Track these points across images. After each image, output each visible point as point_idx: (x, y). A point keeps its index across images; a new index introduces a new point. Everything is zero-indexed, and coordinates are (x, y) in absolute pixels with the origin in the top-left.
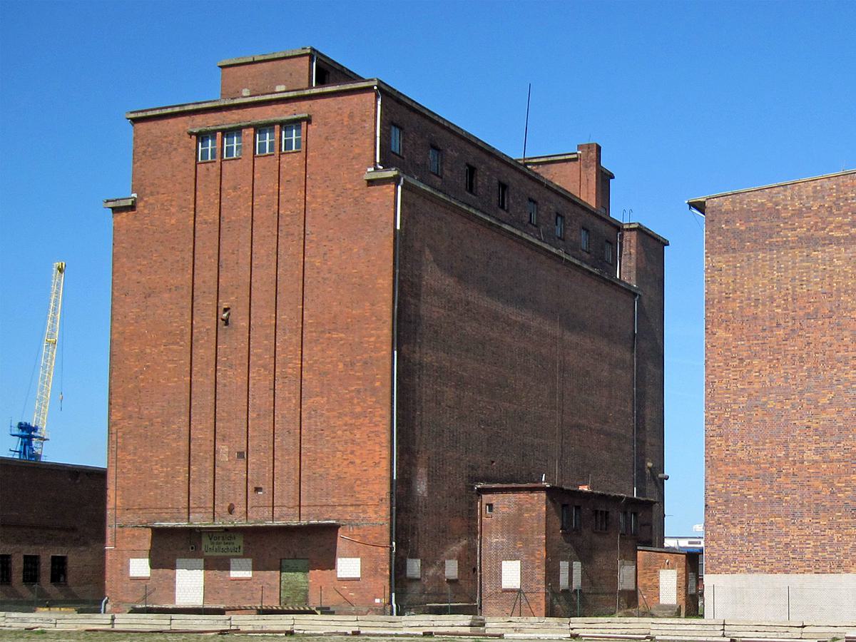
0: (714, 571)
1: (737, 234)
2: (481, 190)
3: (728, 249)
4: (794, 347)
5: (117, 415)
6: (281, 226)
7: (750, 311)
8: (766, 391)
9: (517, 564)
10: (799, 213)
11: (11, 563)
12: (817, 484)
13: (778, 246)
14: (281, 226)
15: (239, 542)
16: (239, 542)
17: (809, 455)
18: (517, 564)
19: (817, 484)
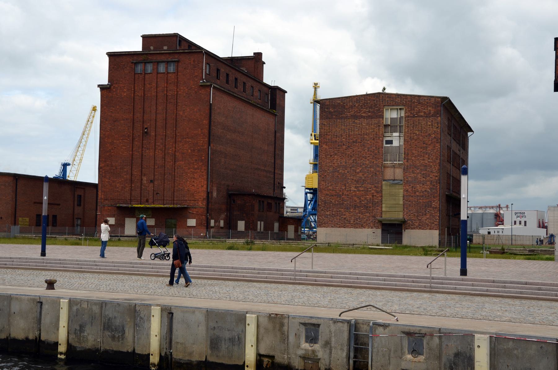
1: (330, 112)
5: (102, 165)
9: (243, 222)
10: (352, 107)
12: (355, 198)
13: (347, 118)
17: (353, 189)
18: (243, 222)
19: (355, 198)
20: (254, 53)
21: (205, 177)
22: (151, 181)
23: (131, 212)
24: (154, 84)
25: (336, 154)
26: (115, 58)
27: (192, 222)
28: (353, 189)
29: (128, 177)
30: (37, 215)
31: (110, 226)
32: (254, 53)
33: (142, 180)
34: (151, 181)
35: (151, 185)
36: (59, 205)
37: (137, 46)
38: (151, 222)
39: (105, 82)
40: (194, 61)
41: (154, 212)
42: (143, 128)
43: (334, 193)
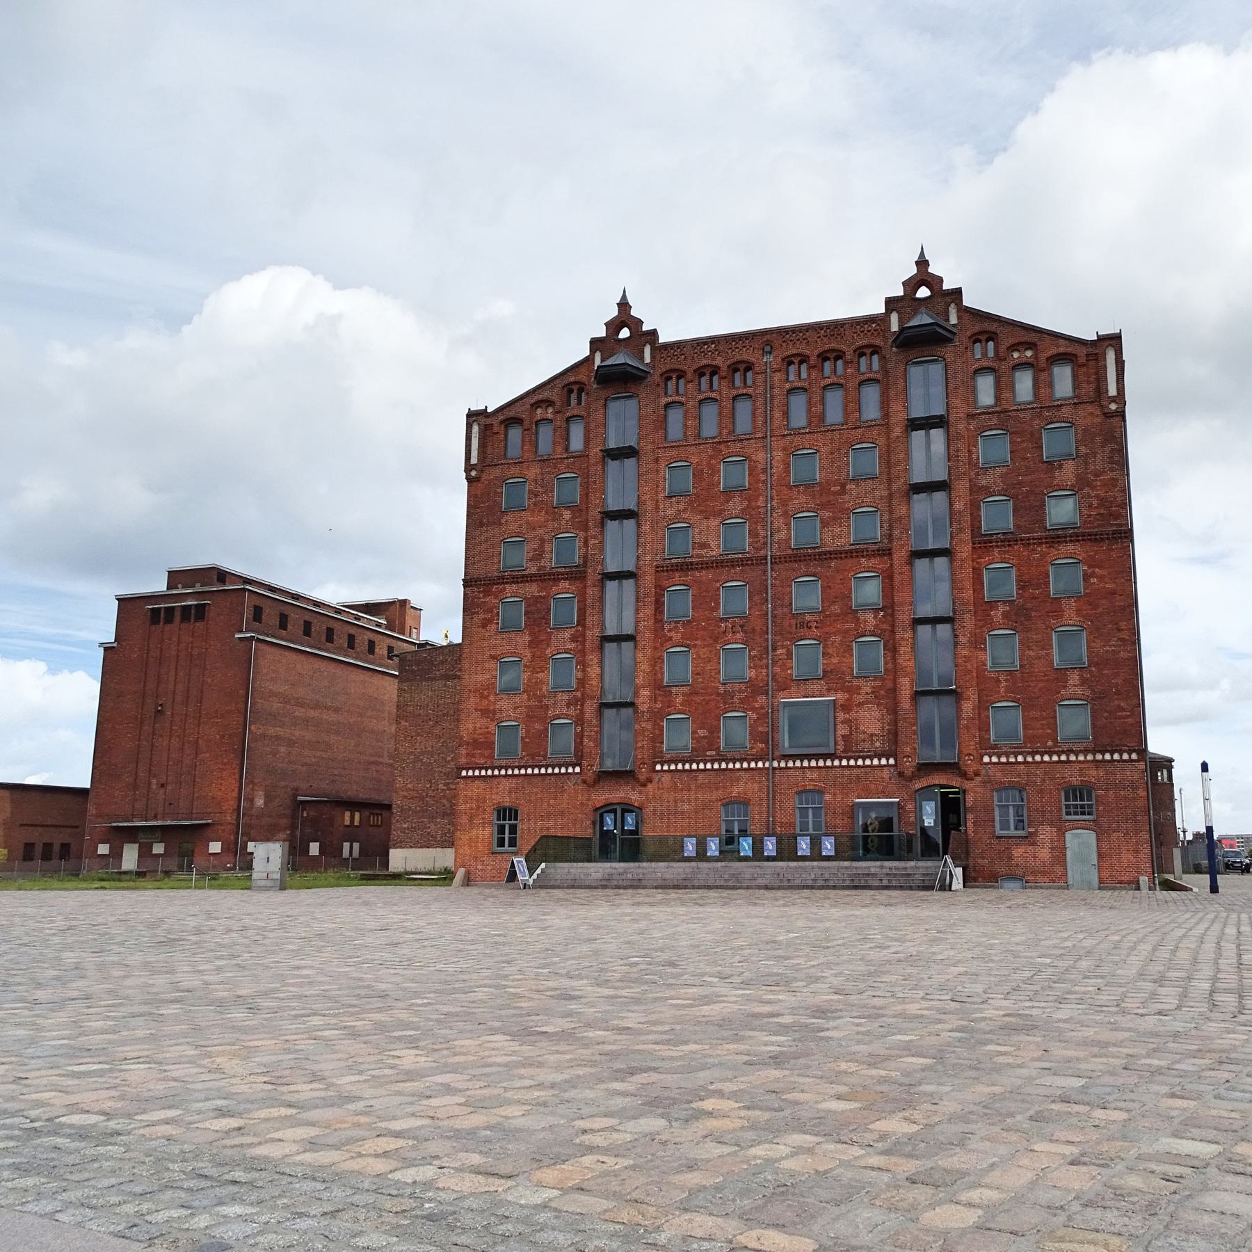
0: (401, 845)
1: (413, 672)
2: (313, 634)
3: (408, 680)
4: (437, 731)
5: (98, 763)
6: (934, 630)
7: (417, 712)
8: (422, 753)
9: (318, 844)
10: (442, 662)
11: (211, 887)
12: (444, 801)
13: (434, 679)
14: (934, 630)
15: (158, 834)
16: (158, 834)
17: (441, 786)
18: (318, 844)
19: (444, 801)
20: (175, 577)
21: (237, 776)
22: (162, 785)
23: (130, 834)
24: (175, 639)
25: (418, 735)
26: (127, 604)
27: (215, 847)
28: (441, 786)
29: (131, 780)
30: (26, 844)
31: (1062, 832)
32: (175, 577)
33: (150, 783)
34: (162, 785)
35: (162, 791)
36: (77, 827)
37: (159, 585)
38: (158, 849)
39: (110, 637)
40: (231, 603)
41: (165, 833)
42: (157, 705)
43: (414, 794)
